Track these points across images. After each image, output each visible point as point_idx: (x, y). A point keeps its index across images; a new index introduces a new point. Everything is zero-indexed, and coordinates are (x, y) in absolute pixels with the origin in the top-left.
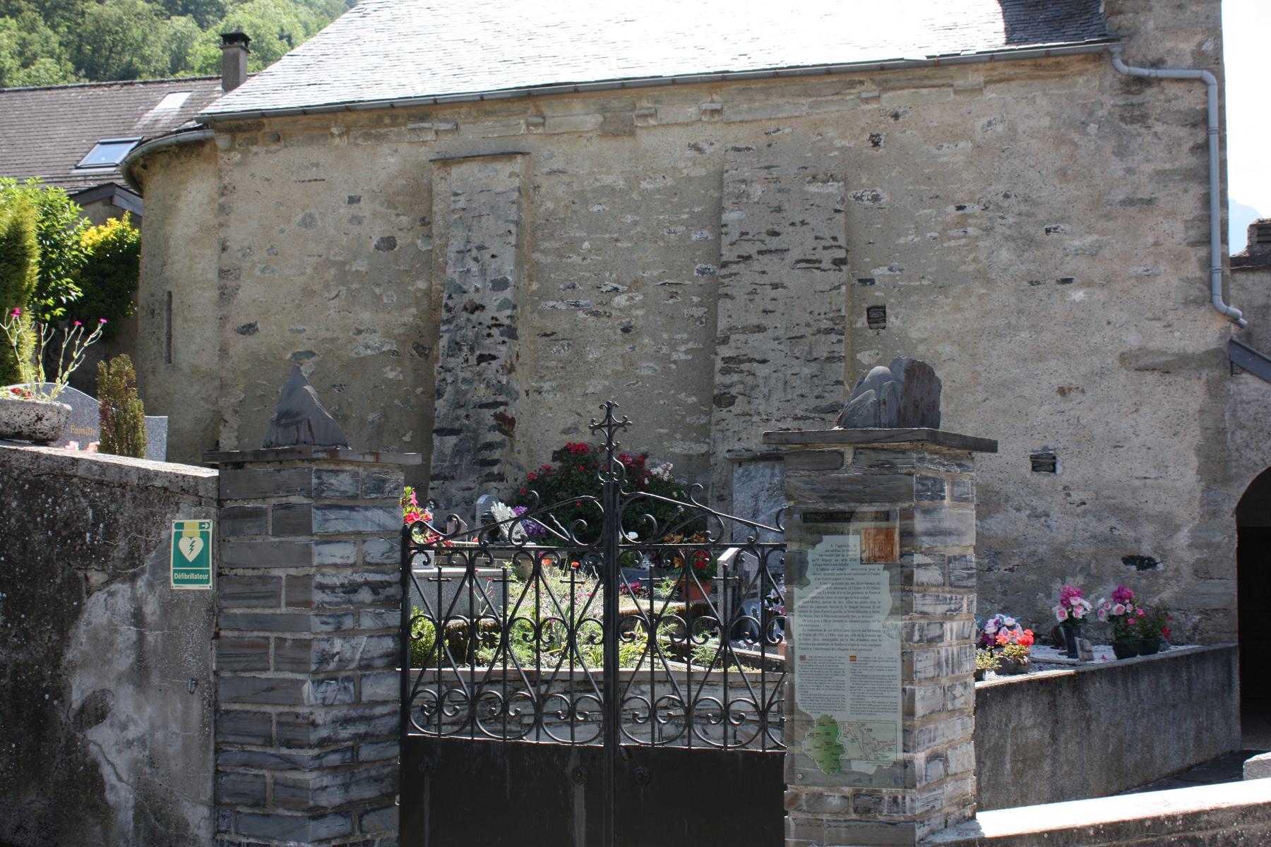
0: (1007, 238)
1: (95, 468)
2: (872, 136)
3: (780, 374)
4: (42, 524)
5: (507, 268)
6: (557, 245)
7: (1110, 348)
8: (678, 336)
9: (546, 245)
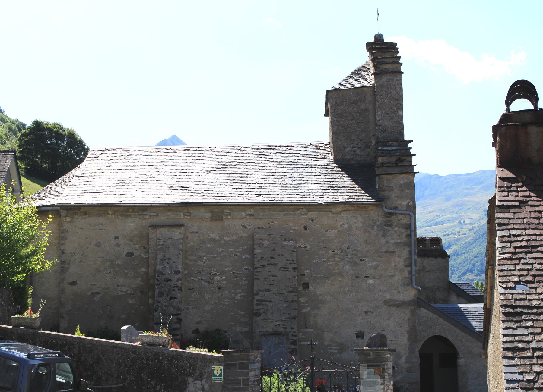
0: (348, 262)
1: (190, 354)
2: (304, 226)
3: (276, 306)
4: (174, 367)
5: (180, 267)
6: (194, 258)
7: (381, 298)
8: (238, 291)
9: (190, 257)
